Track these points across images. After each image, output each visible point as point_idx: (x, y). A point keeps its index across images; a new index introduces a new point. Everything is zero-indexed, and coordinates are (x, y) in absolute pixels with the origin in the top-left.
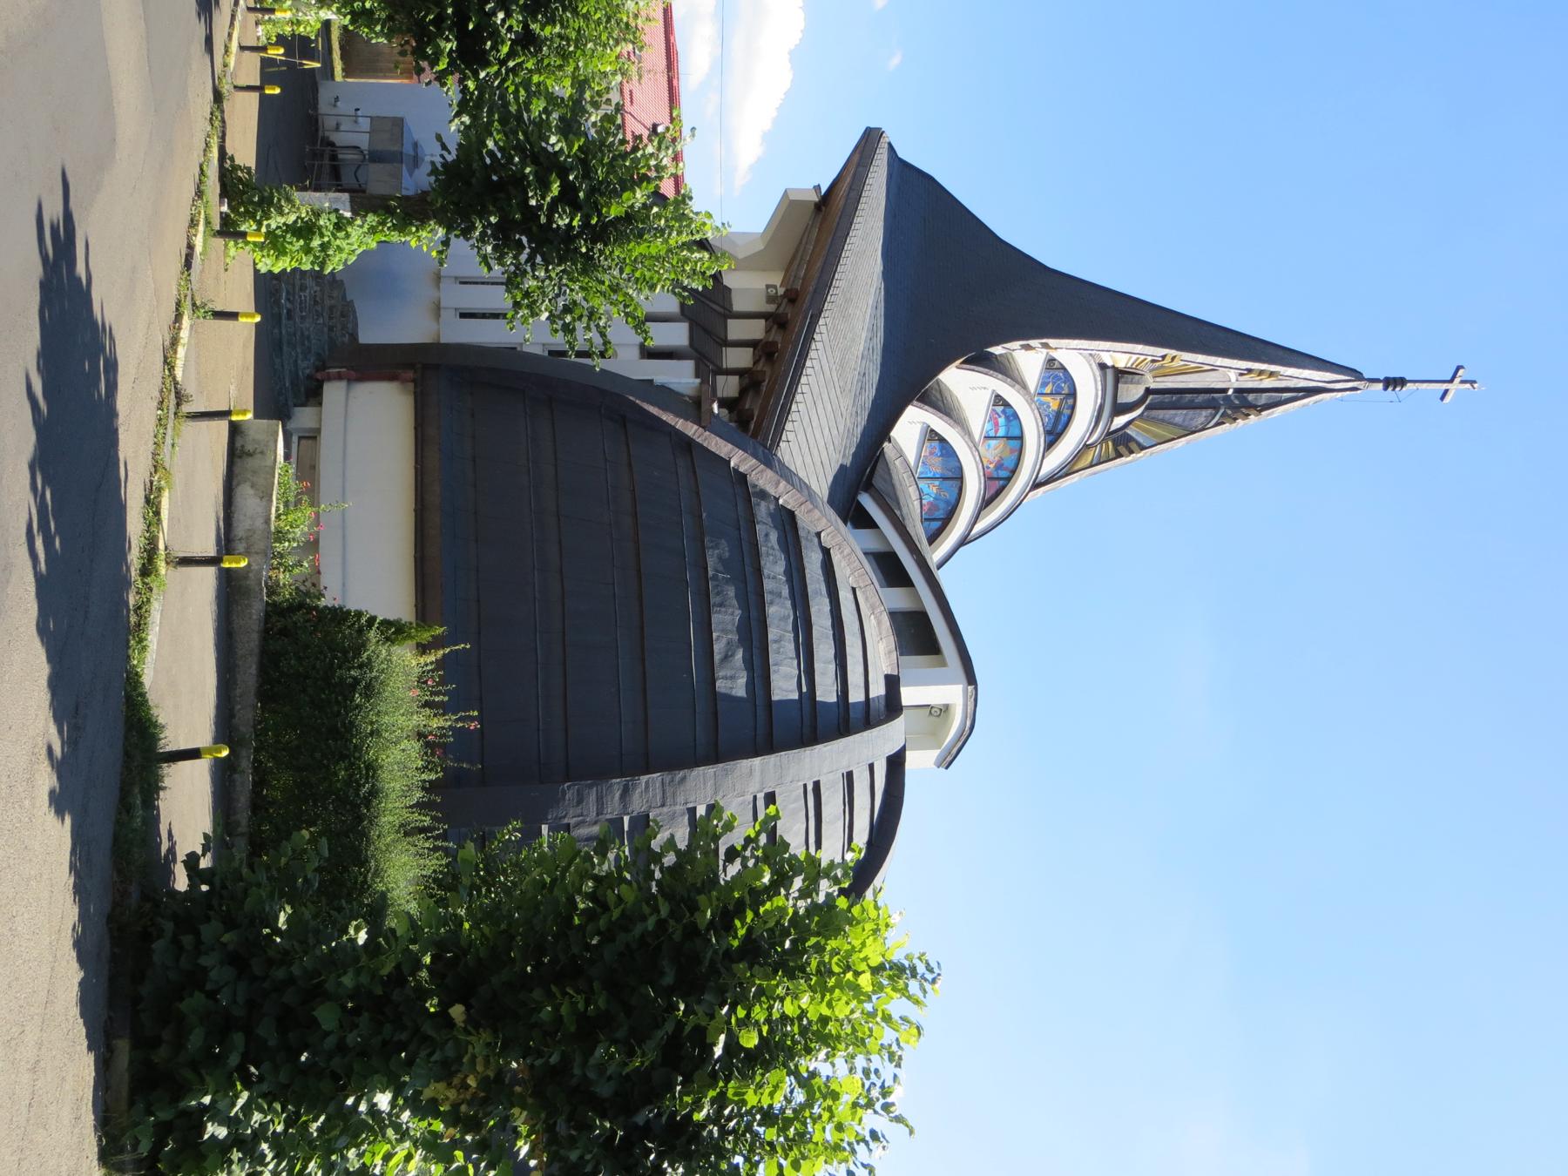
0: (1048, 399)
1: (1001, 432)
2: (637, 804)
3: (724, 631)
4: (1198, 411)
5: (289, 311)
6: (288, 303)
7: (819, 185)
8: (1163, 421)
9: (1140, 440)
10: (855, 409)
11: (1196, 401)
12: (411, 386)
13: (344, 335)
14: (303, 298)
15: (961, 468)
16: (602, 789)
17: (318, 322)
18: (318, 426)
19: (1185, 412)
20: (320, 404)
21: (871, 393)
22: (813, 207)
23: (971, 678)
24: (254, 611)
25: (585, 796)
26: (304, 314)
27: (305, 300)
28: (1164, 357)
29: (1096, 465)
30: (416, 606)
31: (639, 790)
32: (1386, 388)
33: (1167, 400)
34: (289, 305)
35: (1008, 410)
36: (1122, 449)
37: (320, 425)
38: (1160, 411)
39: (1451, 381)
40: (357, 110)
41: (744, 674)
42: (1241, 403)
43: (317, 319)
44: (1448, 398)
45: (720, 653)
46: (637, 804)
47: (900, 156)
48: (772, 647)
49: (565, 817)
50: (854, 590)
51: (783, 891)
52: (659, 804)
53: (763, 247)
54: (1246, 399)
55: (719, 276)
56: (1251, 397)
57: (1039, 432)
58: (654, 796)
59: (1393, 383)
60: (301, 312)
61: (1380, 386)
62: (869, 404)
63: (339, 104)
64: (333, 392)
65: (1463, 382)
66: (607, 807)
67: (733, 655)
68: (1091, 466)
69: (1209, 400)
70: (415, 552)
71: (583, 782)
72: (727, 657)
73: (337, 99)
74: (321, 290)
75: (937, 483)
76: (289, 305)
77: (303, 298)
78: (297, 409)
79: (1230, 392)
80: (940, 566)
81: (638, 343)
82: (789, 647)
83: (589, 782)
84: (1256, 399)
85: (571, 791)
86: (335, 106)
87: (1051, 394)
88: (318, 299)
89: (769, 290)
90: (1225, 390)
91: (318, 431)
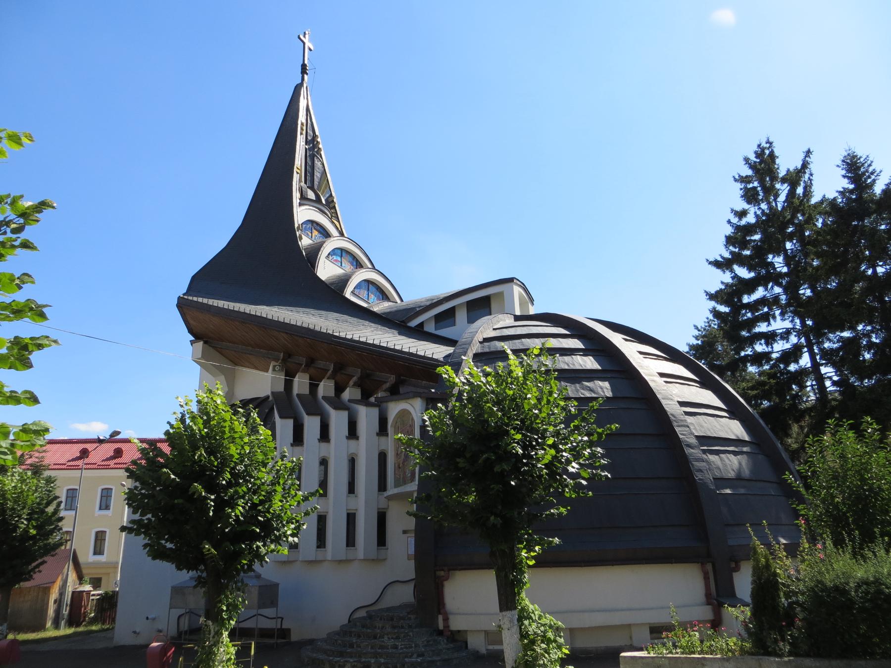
0: (313, 235)
1: (339, 259)
2: (693, 441)
3: (577, 391)
4: (315, 165)
5: (419, 656)
6: (414, 657)
7: (190, 341)
8: (319, 183)
9: (328, 195)
10: (361, 326)
11: (310, 164)
12: (451, 572)
13: (410, 619)
14: (403, 646)
15: (365, 280)
16: (693, 459)
17: (412, 635)
18: (484, 632)
19: (315, 171)
20: (466, 631)
21: (346, 317)
22: (206, 345)
23: (510, 280)
24: (813, 665)
25: (698, 468)
26: (413, 645)
27: (404, 645)
28: (297, 173)
29: (337, 216)
30: (613, 565)
31: (686, 439)
32: (307, 74)
33: (310, 178)
34: (415, 656)
35: (331, 254)
36: (331, 205)
37: (482, 631)
38: (315, 183)
39: (304, 43)
40: (147, 618)
41: (596, 381)
42: (312, 143)
43: (410, 636)
44: (312, 48)
45: (591, 394)
46: (693, 441)
47: (185, 292)
48: (572, 367)
49: (710, 479)
50: (494, 329)
51: (262, 423)
52: (688, 429)
53: (223, 376)
54: (310, 140)
55: (243, 402)
56: (309, 138)
57: (342, 240)
58: (685, 431)
59: (304, 69)
60: (412, 647)
61: (305, 76)
62: (356, 319)
63: (138, 631)
64: (457, 624)
65: (304, 37)
66: (699, 456)
67: (589, 387)
68: (339, 222)
69: (310, 158)
70: (610, 565)
71: (692, 469)
72: (591, 390)
73: (135, 632)
74: (387, 635)
75: (370, 294)
76: (415, 656)
77: (403, 646)
78: (469, 646)
79: (307, 147)
80: (402, 300)
81: (346, 440)
82: (567, 359)
83: (691, 466)
84: (310, 136)
85: (698, 475)
86: (138, 634)
87: (312, 233)
88: (395, 637)
89: (277, 370)
90: (306, 149)
91: (485, 631)
